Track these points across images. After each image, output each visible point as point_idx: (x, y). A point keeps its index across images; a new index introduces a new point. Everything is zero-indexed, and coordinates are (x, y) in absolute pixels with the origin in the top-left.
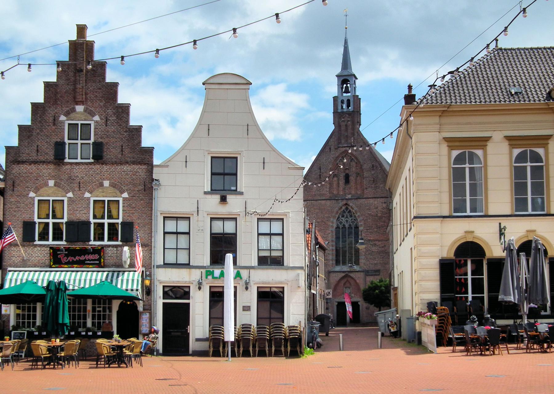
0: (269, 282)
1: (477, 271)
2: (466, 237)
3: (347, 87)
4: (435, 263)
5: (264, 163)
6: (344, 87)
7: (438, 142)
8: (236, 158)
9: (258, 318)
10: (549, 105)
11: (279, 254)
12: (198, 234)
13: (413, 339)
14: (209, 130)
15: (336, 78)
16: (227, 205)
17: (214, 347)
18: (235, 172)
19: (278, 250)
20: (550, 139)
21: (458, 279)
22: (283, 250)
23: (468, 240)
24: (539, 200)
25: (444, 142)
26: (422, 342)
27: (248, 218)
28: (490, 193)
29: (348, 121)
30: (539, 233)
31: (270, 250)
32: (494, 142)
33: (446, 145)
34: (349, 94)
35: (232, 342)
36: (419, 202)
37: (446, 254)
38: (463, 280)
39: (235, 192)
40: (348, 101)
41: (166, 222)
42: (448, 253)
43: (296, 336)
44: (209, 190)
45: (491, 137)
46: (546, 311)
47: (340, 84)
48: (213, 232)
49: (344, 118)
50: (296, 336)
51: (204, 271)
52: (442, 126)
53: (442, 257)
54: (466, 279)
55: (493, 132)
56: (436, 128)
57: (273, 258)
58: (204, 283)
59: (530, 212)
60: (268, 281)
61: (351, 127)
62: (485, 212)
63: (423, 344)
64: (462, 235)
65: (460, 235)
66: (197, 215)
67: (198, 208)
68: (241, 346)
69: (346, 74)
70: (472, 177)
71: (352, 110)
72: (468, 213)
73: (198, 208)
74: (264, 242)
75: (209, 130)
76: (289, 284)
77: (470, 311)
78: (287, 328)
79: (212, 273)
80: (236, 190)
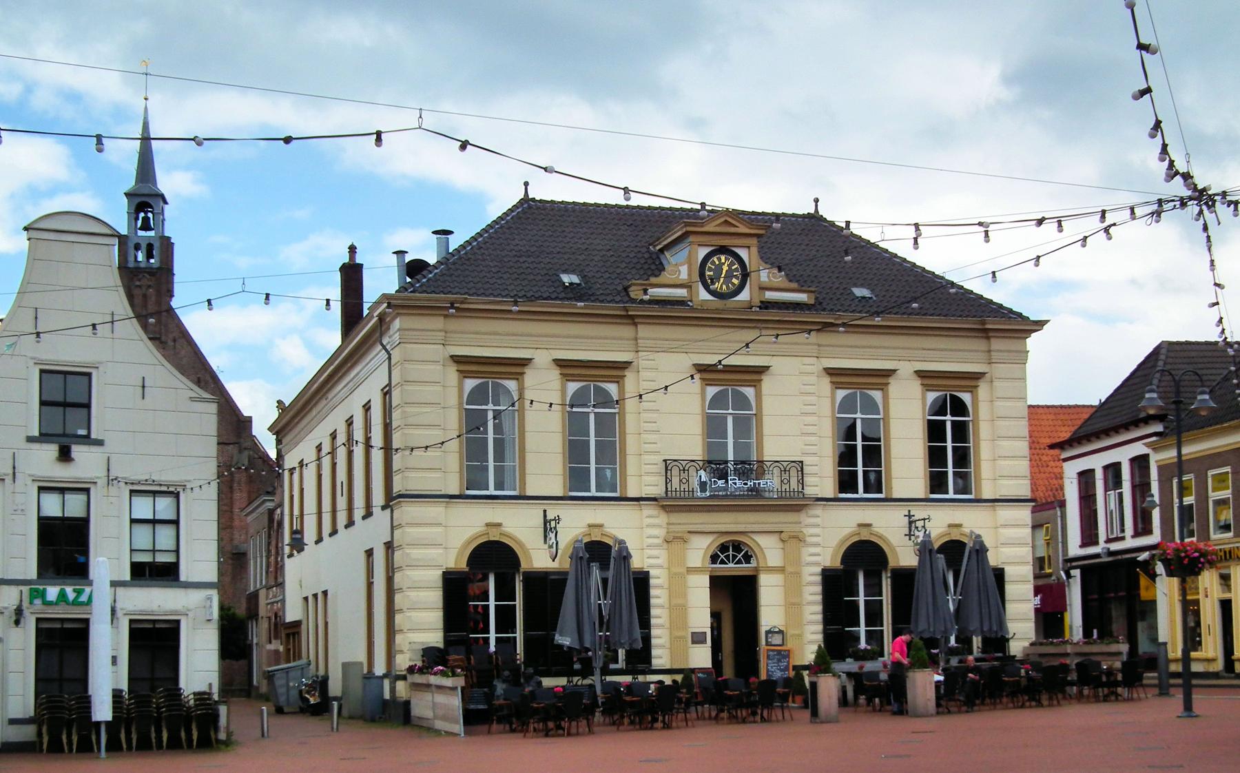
0: (152, 611)
1: (505, 592)
2: (488, 533)
3: (146, 219)
4: (435, 576)
5: (143, 387)
6: (141, 219)
7: (441, 363)
8: (89, 375)
9: (130, 679)
10: (627, 311)
11: (169, 558)
12: (13, 517)
13: (381, 716)
14: (36, 318)
15: (126, 200)
16: (72, 464)
17: (50, 733)
18: (85, 401)
19: (168, 551)
20: (627, 368)
21: (480, 607)
22: (177, 551)
23: (492, 539)
24: (608, 473)
25: (451, 362)
26: (412, 718)
27: (113, 490)
28: (529, 457)
29: (149, 287)
30: (608, 530)
31: (154, 551)
32: (538, 369)
33: (456, 368)
34: (152, 233)
35: (107, 723)
36: (406, 468)
37: (454, 563)
38: (480, 609)
39: (87, 440)
40: (150, 247)
41: (42, 495)
42: (455, 558)
43: (210, 711)
44: (36, 434)
45: (531, 359)
46: (617, 662)
47: (133, 211)
48: (41, 515)
49: (139, 280)
50: (210, 711)
51: (25, 589)
52: (448, 335)
53: (446, 568)
54: (487, 608)
55: (534, 350)
56: (439, 338)
57: (157, 566)
58: (26, 612)
59: (593, 492)
60: (150, 610)
61: (153, 298)
62: (621, 492)
63: (415, 721)
64: (583, 530)
65: (478, 530)
66: (12, 482)
67: (14, 468)
68: (133, 730)
69: (146, 192)
70: (498, 429)
71: (157, 265)
72: (492, 491)
73: (14, 468)
74: (143, 537)
75: (36, 318)
76: (191, 614)
77: (497, 664)
78: (192, 696)
79: (43, 594)
80: (88, 436)
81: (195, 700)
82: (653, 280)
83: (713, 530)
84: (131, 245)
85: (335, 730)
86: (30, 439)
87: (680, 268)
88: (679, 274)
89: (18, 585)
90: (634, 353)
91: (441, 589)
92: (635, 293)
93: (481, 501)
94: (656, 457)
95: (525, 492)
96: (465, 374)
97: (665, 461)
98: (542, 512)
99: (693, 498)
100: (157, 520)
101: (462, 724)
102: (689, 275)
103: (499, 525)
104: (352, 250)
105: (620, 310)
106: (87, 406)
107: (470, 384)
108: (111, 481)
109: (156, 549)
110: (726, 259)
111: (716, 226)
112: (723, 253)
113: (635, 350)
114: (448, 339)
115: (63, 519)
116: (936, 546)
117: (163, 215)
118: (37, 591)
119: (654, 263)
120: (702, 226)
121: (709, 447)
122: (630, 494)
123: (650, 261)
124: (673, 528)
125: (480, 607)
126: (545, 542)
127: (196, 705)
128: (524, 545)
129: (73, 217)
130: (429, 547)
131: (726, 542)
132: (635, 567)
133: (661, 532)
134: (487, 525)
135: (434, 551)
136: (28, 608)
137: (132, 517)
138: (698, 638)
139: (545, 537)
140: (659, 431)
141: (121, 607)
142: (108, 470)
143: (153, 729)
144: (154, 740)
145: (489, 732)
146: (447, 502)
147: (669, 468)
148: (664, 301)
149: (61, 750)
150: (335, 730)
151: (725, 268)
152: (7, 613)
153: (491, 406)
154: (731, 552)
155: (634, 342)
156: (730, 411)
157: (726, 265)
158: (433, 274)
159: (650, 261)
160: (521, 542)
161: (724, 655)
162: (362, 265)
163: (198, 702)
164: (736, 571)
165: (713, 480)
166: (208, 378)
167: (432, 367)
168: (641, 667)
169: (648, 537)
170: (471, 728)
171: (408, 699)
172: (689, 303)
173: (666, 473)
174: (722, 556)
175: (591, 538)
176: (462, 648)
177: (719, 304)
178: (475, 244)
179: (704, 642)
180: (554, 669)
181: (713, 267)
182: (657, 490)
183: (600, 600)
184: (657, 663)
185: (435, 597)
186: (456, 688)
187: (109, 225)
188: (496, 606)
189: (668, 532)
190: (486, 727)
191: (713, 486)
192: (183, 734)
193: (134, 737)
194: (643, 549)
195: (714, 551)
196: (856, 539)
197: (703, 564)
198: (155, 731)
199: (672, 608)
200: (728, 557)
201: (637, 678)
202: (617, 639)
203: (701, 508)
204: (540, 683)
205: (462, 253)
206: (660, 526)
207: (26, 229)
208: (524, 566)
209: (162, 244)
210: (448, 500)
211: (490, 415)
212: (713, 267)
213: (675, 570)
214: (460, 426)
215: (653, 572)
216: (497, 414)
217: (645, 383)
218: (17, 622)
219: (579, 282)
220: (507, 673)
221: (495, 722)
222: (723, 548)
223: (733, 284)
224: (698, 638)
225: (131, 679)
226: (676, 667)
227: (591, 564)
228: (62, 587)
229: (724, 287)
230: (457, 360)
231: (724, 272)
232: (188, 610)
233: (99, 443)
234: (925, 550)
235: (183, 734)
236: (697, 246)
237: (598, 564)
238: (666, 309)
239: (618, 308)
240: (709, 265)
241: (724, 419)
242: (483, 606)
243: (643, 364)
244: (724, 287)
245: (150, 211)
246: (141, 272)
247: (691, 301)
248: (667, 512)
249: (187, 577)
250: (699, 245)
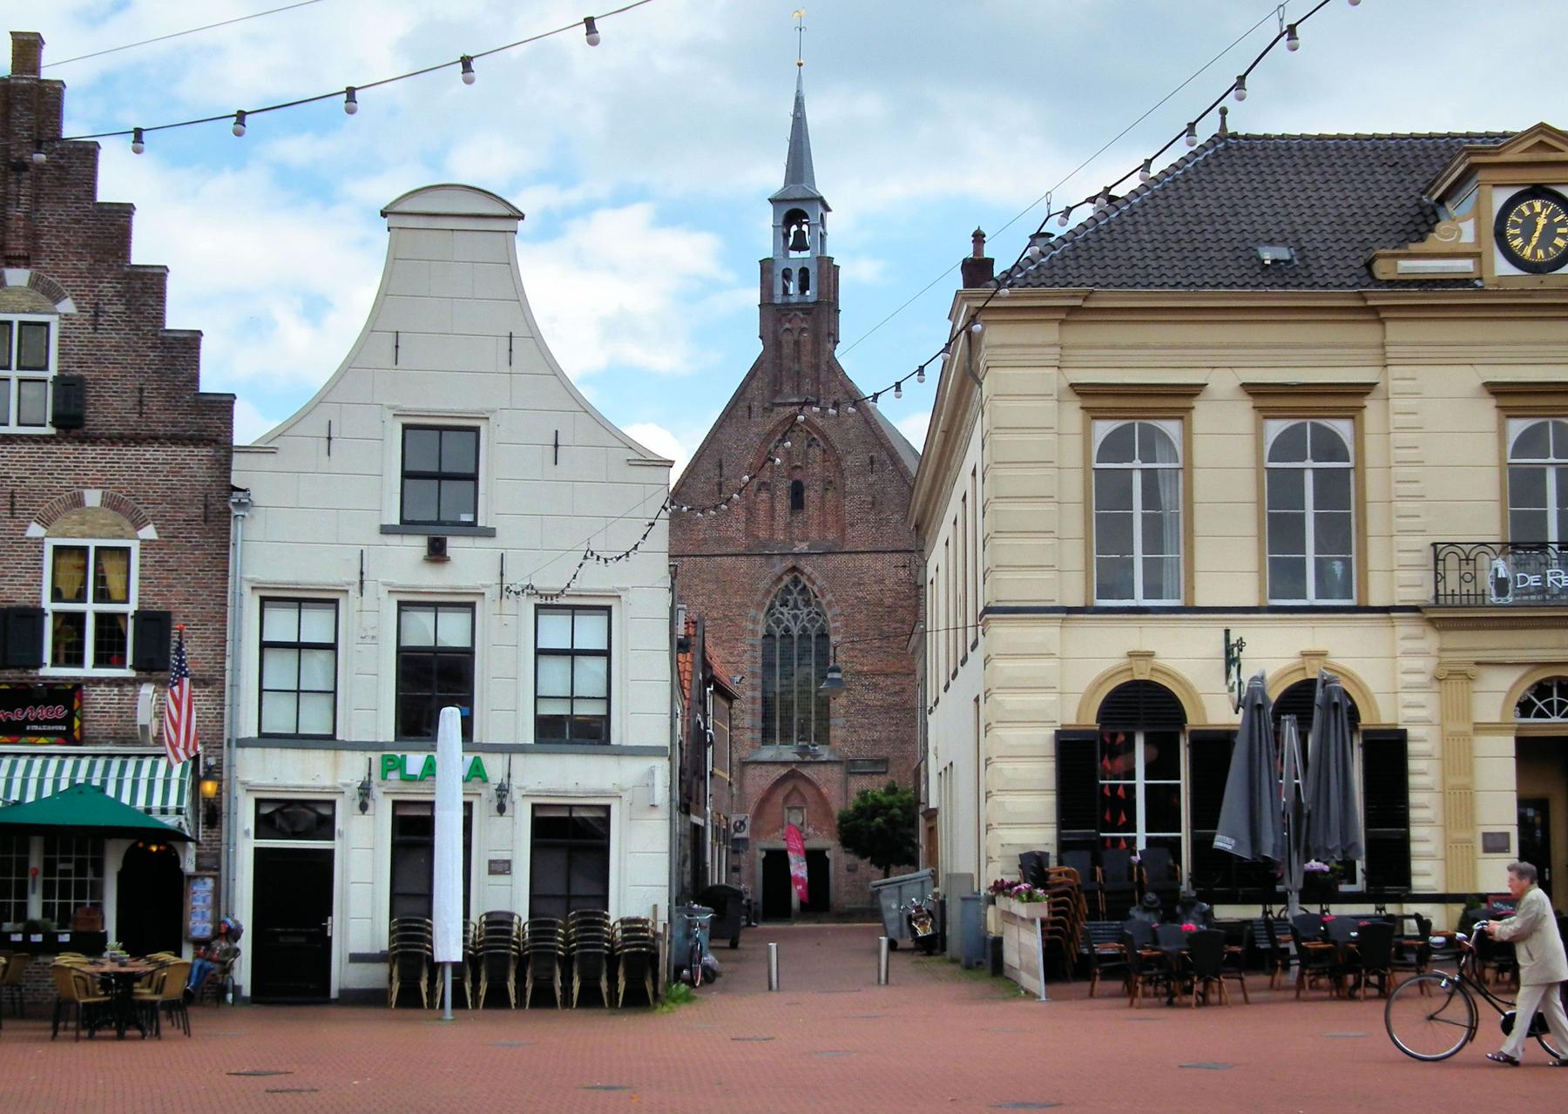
0: (566, 792)
1: (1162, 765)
2: (1132, 669)
4: (1043, 738)
5: (556, 446)
8: (476, 430)
10: (1365, 299)
11: (597, 709)
12: (360, 647)
15: (770, 207)
16: (447, 568)
21: (1107, 787)
22: (608, 699)
23: (1138, 677)
24: (1338, 567)
26: (1005, 967)
27: (509, 604)
29: (803, 330)
31: (572, 698)
33: (1079, 404)
34: (806, 254)
35: (455, 965)
36: (997, 566)
37: (1075, 716)
38: (1121, 792)
39: (472, 529)
40: (804, 272)
41: (268, 613)
42: (1078, 710)
44: (396, 521)
46: (1353, 881)
49: (790, 321)
51: (376, 757)
52: (1067, 352)
53: (1062, 725)
54: (1131, 790)
58: (376, 791)
59: (1311, 599)
61: (809, 347)
62: (1186, 598)
66: (359, 595)
67: (362, 573)
70: (1151, 498)
72: (1139, 600)
73: (362, 573)
76: (626, 797)
78: (618, 925)
79: (401, 765)
80: (473, 524)
81: (624, 931)
82: (1414, 248)
83: (1522, 659)
84: (778, 272)
85: (883, 982)
86: (386, 530)
87: (1460, 224)
88: (1459, 236)
89: (365, 750)
90: (1380, 368)
91: (1054, 759)
92: (1383, 269)
93: (1120, 616)
94: (1419, 539)
95: (1193, 601)
96: (1094, 414)
97: (1434, 545)
98: (1223, 633)
99: (1484, 606)
100: (304, 643)
101: (1043, 979)
102: (1478, 235)
103: (1150, 655)
104: (979, 238)
105: (1352, 299)
106: (474, 478)
107: (1103, 428)
108: (505, 591)
109: (569, 695)
110: (1544, 206)
111: (1522, 152)
112: (1536, 197)
113: (1381, 363)
114: (1065, 358)
115: (436, 651)
116: (1274, 696)
117: (823, 227)
118: (391, 759)
119: (1426, 222)
120: (1498, 154)
121: (1517, 520)
122: (1375, 601)
123: (1419, 219)
124: (1449, 656)
125: (1121, 789)
126: (1227, 683)
127: (625, 939)
128: (1192, 687)
129: (457, 193)
130: (1033, 691)
131: (1547, 679)
132: (1383, 722)
133: (1427, 664)
134: (1131, 655)
135: (1040, 698)
136: (379, 786)
137: (539, 646)
138: (1494, 843)
139: (1228, 673)
140: (1423, 496)
141: (518, 784)
142: (502, 575)
143: (605, 968)
144: (558, 993)
145: (1091, 995)
146: (1063, 619)
147: (1441, 557)
148: (1428, 281)
149: (418, 1004)
150: (883, 982)
151: (1542, 221)
152: (348, 793)
153: (1137, 463)
154: (1555, 698)
155: (1380, 351)
156: (1552, 460)
157: (1543, 216)
158: (1048, 258)
159: (1419, 219)
160: (1365, 685)
161: (1554, 871)
162: (993, 260)
163: (626, 935)
164: (1530, 729)
165: (1518, 575)
166: (884, 456)
167: (1039, 404)
168: (1390, 890)
169: (1404, 673)
170: (1060, 987)
171: (999, 935)
172: (1478, 283)
173: (1436, 564)
174: (1540, 704)
175: (1306, 674)
176: (1086, 856)
177: (1531, 281)
178: (1126, 208)
179: (1505, 848)
180: (1241, 891)
181: (1520, 221)
182: (1421, 593)
183: (1297, 779)
184: (1420, 884)
185: (1044, 771)
186: (1033, 921)
187: (500, 198)
188: (1147, 786)
189: (1439, 664)
190: (1086, 986)
191: (1519, 586)
192: (604, 984)
193: (484, 986)
194: (1396, 693)
195: (1524, 695)
196: (1298, 678)
197: (1502, 717)
198: (562, 979)
199: (1447, 791)
200: (1549, 705)
201: (1384, 909)
202: (1321, 844)
203: (1496, 623)
204: (1210, 913)
205: (1102, 223)
206: (1425, 654)
207: (384, 214)
208: (1193, 721)
209: (820, 267)
210: (1064, 615)
211: (1137, 479)
212: (1520, 221)
213: (1452, 727)
214: (1085, 496)
215: (1412, 732)
216: (1150, 477)
217: (1397, 417)
218: (364, 807)
219: (1287, 257)
220: (1151, 896)
221: (1098, 978)
222: (1541, 689)
223: (1557, 248)
224: (1494, 843)
225: (536, 897)
226: (1453, 891)
227: (1283, 717)
228: (478, 754)
229: (1540, 253)
230: (1082, 390)
231: (1540, 227)
232: (622, 790)
233: (490, 533)
234: (1252, 703)
235: (604, 984)
236: (1490, 187)
237: (1295, 717)
238: (1430, 294)
239: (1346, 297)
240: (1513, 217)
241: (1540, 473)
242: (1125, 786)
243: (1395, 386)
244: (1540, 253)
245: (806, 223)
246: (791, 310)
247: (1480, 279)
248: (1439, 630)
249: (621, 739)
250: (1494, 185)
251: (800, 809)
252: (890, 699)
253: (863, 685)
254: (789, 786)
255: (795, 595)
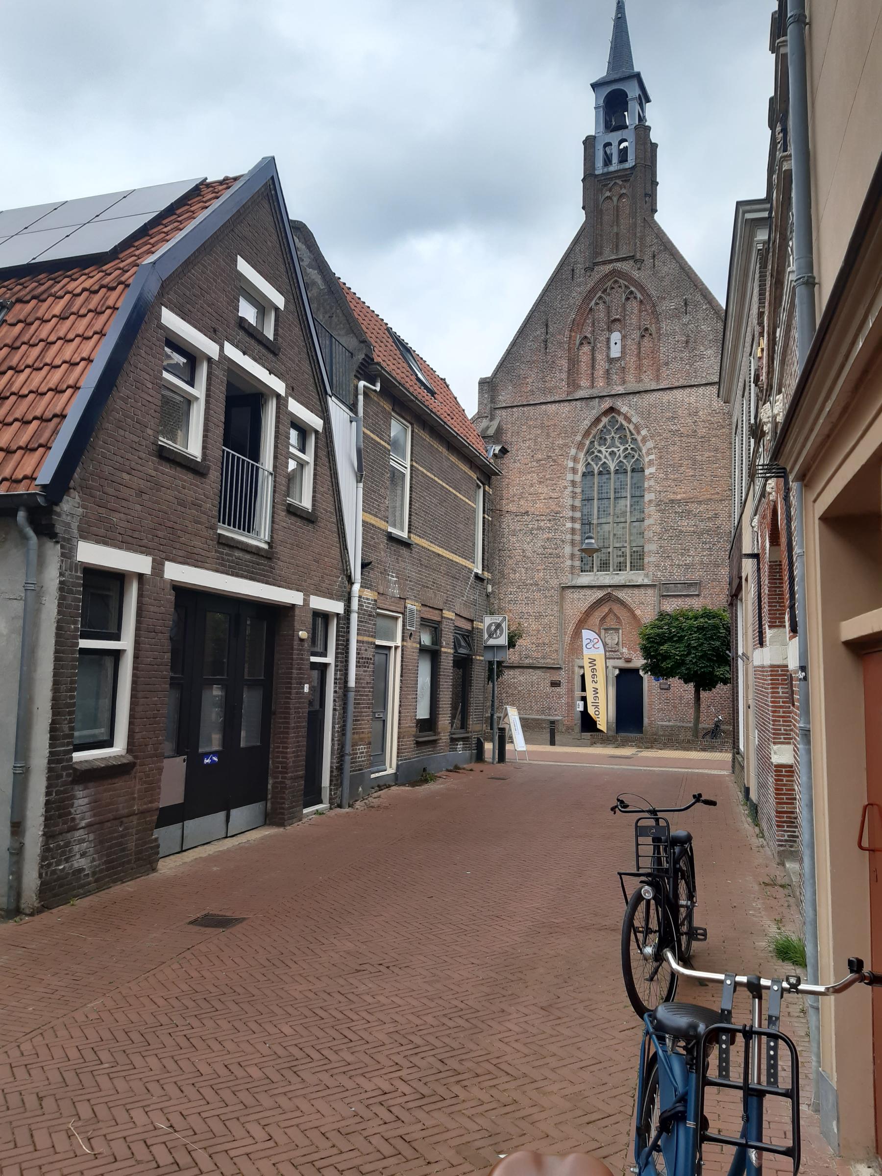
251: (617, 630)
252: (702, 525)
253: (676, 513)
254: (605, 609)
255: (613, 434)
